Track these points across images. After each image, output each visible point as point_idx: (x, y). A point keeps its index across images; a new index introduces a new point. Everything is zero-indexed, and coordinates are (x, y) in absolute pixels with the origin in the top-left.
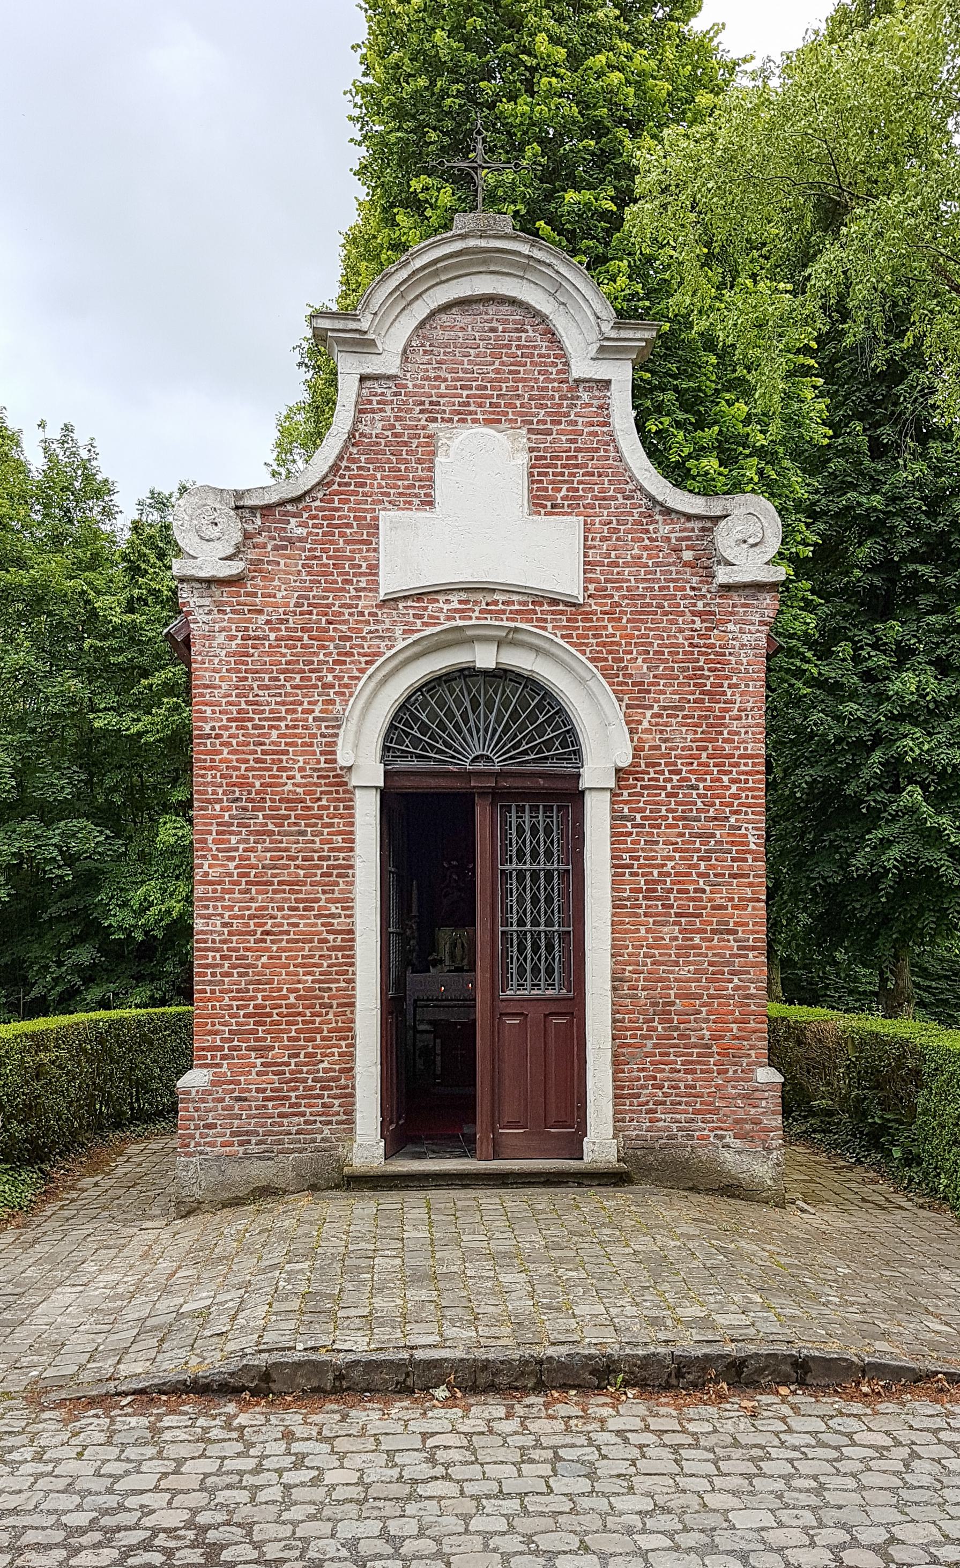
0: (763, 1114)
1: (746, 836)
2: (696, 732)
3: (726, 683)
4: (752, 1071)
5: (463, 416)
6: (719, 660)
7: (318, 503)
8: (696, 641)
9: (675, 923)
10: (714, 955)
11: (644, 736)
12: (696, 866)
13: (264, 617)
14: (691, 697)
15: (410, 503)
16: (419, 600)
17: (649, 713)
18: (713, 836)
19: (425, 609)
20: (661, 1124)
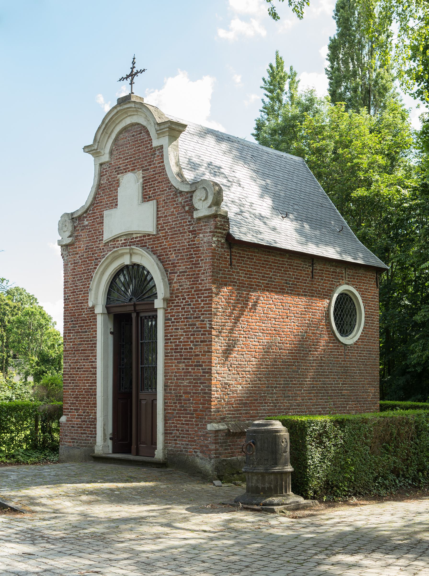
0: (209, 443)
1: (205, 324)
2: (190, 281)
3: (200, 259)
4: (206, 425)
5: (126, 170)
6: (197, 249)
7: (91, 212)
8: (190, 243)
9: (184, 362)
10: (195, 376)
11: (175, 285)
12: (190, 338)
13: (78, 255)
14: (188, 267)
15: (112, 206)
16: (114, 241)
17: (176, 275)
18: (195, 325)
19: (115, 244)
20: (178, 445)
